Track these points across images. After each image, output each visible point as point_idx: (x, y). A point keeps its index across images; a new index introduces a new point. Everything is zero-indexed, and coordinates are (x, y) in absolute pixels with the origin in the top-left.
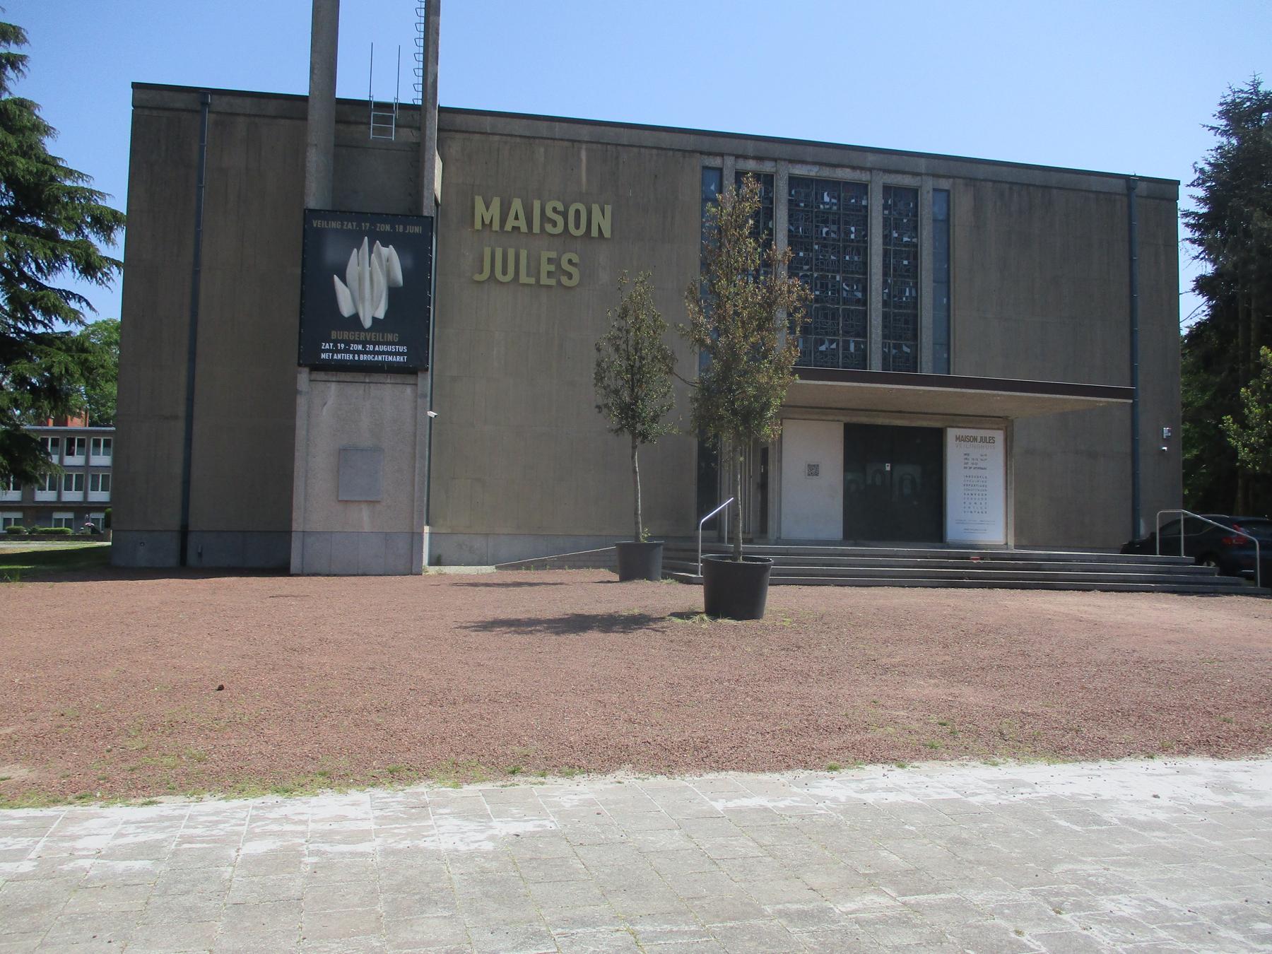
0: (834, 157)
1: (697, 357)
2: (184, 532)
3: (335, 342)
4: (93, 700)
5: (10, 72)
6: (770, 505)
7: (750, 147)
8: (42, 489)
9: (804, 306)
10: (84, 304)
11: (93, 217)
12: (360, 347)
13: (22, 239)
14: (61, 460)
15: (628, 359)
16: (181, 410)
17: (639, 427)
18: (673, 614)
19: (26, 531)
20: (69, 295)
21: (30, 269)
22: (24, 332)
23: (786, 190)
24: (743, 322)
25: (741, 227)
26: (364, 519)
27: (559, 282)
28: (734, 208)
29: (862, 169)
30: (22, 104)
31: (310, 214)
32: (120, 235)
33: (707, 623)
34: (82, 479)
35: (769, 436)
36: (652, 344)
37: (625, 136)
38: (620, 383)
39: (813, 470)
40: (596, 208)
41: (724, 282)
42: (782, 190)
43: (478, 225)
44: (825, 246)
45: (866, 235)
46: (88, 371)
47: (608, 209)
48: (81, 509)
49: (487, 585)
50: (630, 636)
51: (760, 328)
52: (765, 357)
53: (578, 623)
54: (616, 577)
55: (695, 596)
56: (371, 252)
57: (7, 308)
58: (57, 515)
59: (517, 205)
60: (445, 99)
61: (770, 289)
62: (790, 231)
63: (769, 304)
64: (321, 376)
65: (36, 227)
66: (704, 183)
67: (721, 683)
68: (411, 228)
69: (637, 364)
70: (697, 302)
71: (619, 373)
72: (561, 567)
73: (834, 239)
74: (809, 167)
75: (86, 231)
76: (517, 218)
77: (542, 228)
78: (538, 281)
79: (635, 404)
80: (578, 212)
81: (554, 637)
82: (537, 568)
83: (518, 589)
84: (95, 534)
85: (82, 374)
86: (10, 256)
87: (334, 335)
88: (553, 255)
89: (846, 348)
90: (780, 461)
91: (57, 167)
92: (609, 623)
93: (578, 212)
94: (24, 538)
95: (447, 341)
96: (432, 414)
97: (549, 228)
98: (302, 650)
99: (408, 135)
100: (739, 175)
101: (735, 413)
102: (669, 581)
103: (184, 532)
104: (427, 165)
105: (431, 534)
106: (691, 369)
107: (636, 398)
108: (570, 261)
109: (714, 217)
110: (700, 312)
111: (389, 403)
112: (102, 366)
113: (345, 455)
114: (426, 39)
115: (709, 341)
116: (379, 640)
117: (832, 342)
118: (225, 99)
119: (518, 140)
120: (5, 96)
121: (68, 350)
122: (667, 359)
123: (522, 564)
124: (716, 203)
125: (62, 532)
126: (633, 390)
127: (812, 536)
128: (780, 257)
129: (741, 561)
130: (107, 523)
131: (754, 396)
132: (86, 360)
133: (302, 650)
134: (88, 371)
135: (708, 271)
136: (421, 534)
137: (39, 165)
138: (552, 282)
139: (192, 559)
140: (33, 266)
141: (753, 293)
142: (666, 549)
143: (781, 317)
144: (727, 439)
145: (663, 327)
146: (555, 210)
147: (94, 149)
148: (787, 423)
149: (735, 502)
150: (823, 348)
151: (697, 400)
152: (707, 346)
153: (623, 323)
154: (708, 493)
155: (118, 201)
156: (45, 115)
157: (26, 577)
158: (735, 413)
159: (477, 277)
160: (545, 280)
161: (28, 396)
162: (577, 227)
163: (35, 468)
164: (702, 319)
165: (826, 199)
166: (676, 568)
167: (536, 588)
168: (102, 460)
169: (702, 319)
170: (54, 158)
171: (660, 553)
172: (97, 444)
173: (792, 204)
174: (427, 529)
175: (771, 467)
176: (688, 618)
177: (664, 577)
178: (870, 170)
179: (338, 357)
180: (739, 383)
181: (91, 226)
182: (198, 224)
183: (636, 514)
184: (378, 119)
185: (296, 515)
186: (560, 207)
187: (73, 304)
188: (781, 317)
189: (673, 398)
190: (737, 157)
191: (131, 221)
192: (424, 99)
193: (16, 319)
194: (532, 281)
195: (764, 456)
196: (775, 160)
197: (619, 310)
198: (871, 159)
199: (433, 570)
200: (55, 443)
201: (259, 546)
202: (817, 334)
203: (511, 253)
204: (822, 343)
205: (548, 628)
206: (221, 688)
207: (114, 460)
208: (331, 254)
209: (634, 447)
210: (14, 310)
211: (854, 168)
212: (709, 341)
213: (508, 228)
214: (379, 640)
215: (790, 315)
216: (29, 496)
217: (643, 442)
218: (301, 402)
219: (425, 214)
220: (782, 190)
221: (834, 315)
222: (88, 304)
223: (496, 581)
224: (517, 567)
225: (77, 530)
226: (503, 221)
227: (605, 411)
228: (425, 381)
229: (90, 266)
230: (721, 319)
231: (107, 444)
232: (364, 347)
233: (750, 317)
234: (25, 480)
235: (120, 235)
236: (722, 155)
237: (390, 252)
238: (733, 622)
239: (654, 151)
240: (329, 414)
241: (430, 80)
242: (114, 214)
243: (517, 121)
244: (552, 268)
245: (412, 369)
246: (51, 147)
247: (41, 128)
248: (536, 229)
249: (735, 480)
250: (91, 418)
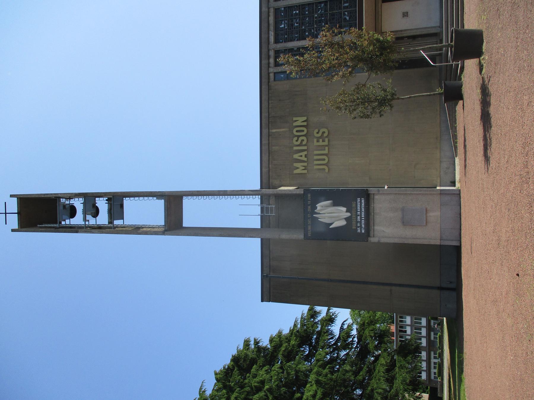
0: (265, 25)
1: (357, 74)
2: (441, 288)
3: (357, 227)
4: (522, 328)
5: (260, 344)
6: (424, 33)
7: (265, 62)
8: (421, 343)
9: (332, 28)
10: (345, 323)
11: (311, 318)
12: (359, 217)
13: (321, 344)
14: (408, 335)
15: (359, 104)
16: (388, 288)
17: (389, 97)
18: (481, 73)
19: (439, 351)
20: (342, 328)
21: (332, 341)
22: (357, 345)
23: (281, 44)
24: (341, 55)
25: (300, 61)
26: (435, 215)
27: (326, 137)
28: (292, 65)
29: (269, 12)
30: (271, 340)
31: (306, 237)
32: (318, 308)
33: (485, 57)
34: (416, 327)
35: (392, 37)
36: (351, 95)
37: (265, 114)
38: (369, 107)
39: (405, 15)
40: (295, 124)
41: (324, 66)
42: (280, 46)
43: (305, 171)
44: (303, 23)
45: (297, 6)
46: (372, 322)
47: (295, 119)
48: (429, 329)
49: (465, 160)
50: (492, 93)
51: (342, 47)
52: (355, 43)
53: (486, 119)
54: (461, 102)
55: (470, 64)
56: (319, 214)
57: (348, 351)
58: (432, 338)
59: (296, 156)
60: (258, 187)
61: (326, 45)
62: (297, 40)
63: (331, 45)
64: (371, 233)
65: (316, 338)
66: (281, 80)
67: (518, 46)
68: (310, 197)
69: (361, 100)
70: (333, 76)
71: (365, 108)
72: (456, 128)
73: (299, 20)
74: (270, 35)
75: (317, 321)
76: (301, 156)
77: (305, 145)
78: (326, 146)
79: (379, 100)
80: (297, 131)
81: (493, 128)
82: (456, 138)
83: (467, 146)
84: (441, 324)
85: (374, 325)
86: (327, 348)
87: (354, 228)
88: (315, 140)
89: (347, 7)
90: (401, 31)
91: (293, 330)
92: (485, 103)
93: (297, 131)
94: (442, 351)
95: (355, 183)
96: (386, 187)
97: (304, 143)
98: (499, 240)
99: (272, 200)
100: (277, 64)
101: (381, 54)
102: (462, 77)
103: (441, 288)
104: (283, 192)
105: (440, 186)
106: (362, 76)
107: (376, 100)
108: (318, 133)
109: (297, 73)
110: (337, 75)
111: (382, 205)
112: (370, 317)
113: (405, 223)
114: (236, 195)
115: (350, 69)
116: (494, 207)
117: (344, 14)
118: (265, 269)
119: (270, 157)
120: (269, 346)
121: (364, 330)
122: (359, 88)
123: (454, 145)
124: (291, 73)
125: (440, 337)
126: (372, 101)
127: (438, 13)
128: (311, 42)
129: (453, 43)
130: (436, 319)
131: (374, 46)
132: (367, 323)
133: (499, 240)
134: (372, 322)
135: (319, 73)
136: (441, 190)
137: (293, 336)
138: (327, 140)
139: (453, 286)
140: (331, 340)
141: (327, 52)
142: (446, 80)
143: (337, 39)
144: (395, 56)
145: (344, 91)
146: (297, 141)
147: (286, 317)
148: (384, 30)
149: (423, 50)
150: (348, 18)
151: (376, 72)
152: (352, 70)
153: (343, 108)
154: (421, 63)
155: (305, 308)
156: (275, 333)
157: (461, 351)
158: (381, 54)
159: (327, 171)
160: (326, 143)
161: (383, 345)
162: (303, 131)
163: (413, 345)
164: (341, 73)
165: (283, 26)
166: (455, 75)
167: (467, 138)
168: (408, 320)
169: (341, 73)
170: (290, 330)
171: (447, 82)
172: (401, 321)
173: (286, 41)
174: (438, 188)
175: (405, 35)
176: (482, 66)
177: (461, 79)
178: (269, 8)
179: (363, 226)
180: (368, 54)
181: (314, 319)
182: (313, 279)
183: (430, 95)
184: (267, 212)
185: (433, 242)
186: (296, 138)
187: (345, 327)
188: (337, 39)
189: (376, 83)
190: (269, 67)
191: (312, 303)
192: (258, 195)
193: (352, 348)
194: (327, 148)
195: (401, 38)
196: (269, 50)
197: (338, 110)
198: (264, 9)
199: (458, 185)
200: (401, 337)
201: (449, 257)
202: (341, 22)
203: (316, 157)
204: (345, 19)
205: (488, 132)
206: (518, 275)
207: (409, 315)
208: (321, 229)
209: (398, 99)
210: (349, 348)
211: (269, 16)
212: (350, 69)
213: (305, 159)
214: (494, 207)
215: (336, 35)
216: (424, 349)
217: (396, 95)
218: (383, 240)
219: (303, 192)
220: (280, 46)
221: (333, 15)
222: (345, 321)
223: (463, 157)
224: (456, 148)
225: (439, 331)
226: (304, 161)
227: (382, 113)
228: (372, 191)
229: (330, 320)
230: (340, 65)
231: (401, 317)
232: (359, 215)
233: (338, 52)
234: (418, 349)
235: (318, 308)
236: (269, 73)
237: (319, 206)
238: (484, 44)
239: (270, 102)
240: (388, 228)
241: (251, 193)
242: (309, 310)
243: (263, 158)
244: (321, 140)
245: (367, 195)
246: (286, 331)
247: (280, 333)
248: (305, 148)
249: (413, 50)
250: (390, 323)
